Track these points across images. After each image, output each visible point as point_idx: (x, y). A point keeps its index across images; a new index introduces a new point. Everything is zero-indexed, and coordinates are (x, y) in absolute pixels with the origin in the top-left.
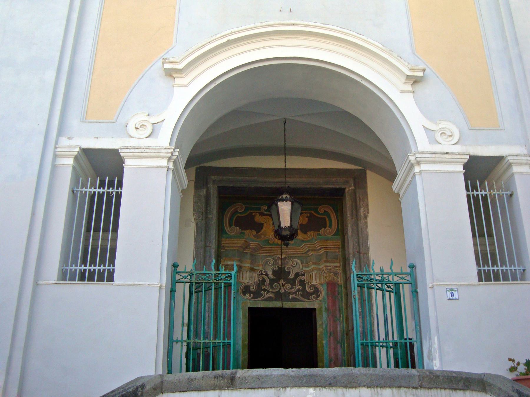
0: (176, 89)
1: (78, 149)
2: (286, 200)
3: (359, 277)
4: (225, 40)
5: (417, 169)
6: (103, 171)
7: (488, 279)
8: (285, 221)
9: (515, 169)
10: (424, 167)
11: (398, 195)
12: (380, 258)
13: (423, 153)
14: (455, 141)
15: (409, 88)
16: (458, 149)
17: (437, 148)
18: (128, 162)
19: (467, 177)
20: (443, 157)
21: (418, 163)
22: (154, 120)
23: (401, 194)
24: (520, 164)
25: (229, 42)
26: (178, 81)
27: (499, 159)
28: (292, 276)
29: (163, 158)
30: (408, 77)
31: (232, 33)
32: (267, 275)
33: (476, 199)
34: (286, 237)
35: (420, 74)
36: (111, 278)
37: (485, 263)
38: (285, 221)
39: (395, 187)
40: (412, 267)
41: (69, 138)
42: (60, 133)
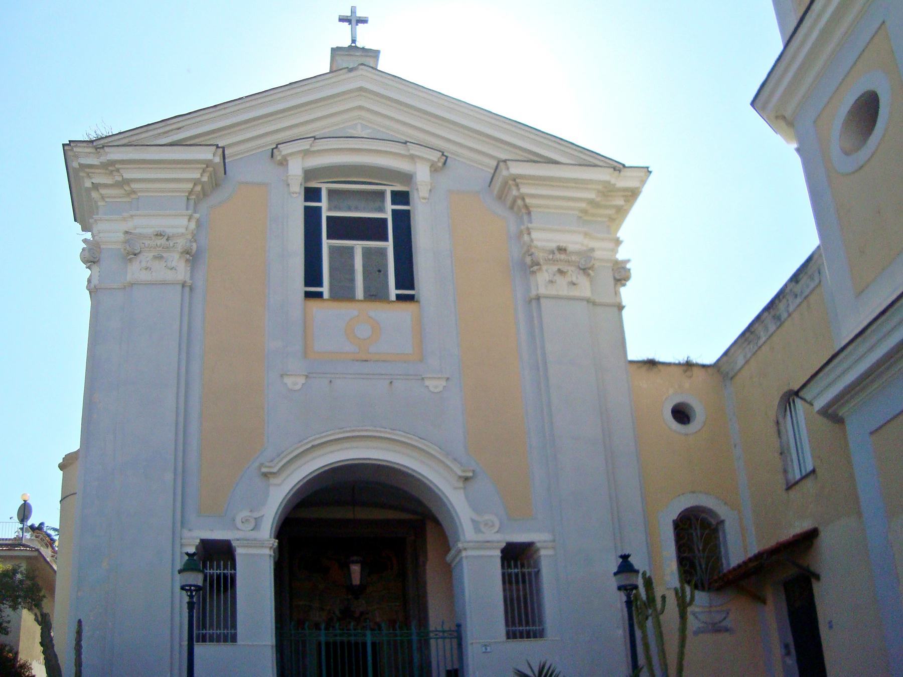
0: (271, 488)
1: (198, 541)
2: (356, 562)
3: (418, 634)
4: (309, 445)
5: (464, 554)
6: (215, 556)
7: (515, 637)
8: (356, 580)
9: (543, 552)
10: (470, 553)
11: (450, 565)
12: (436, 617)
13: (469, 542)
14: (496, 530)
15: (461, 484)
16: (498, 537)
17: (481, 537)
18: (239, 552)
19: (503, 559)
20: (486, 544)
21: (465, 549)
22: (256, 515)
23: (453, 565)
24: (546, 548)
25: (313, 446)
26: (273, 481)
27: (530, 545)
28: (357, 615)
29: (266, 547)
30: (460, 477)
31: (315, 440)
32: (334, 613)
33: (510, 575)
34: (357, 592)
35: (471, 474)
36: (234, 639)
37: (513, 624)
38: (356, 580)
39: (449, 558)
40: (459, 626)
41: (190, 530)
42: (183, 524)
